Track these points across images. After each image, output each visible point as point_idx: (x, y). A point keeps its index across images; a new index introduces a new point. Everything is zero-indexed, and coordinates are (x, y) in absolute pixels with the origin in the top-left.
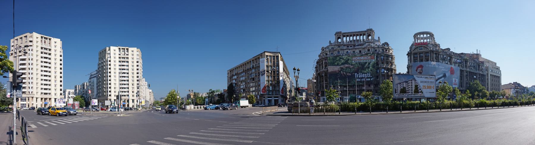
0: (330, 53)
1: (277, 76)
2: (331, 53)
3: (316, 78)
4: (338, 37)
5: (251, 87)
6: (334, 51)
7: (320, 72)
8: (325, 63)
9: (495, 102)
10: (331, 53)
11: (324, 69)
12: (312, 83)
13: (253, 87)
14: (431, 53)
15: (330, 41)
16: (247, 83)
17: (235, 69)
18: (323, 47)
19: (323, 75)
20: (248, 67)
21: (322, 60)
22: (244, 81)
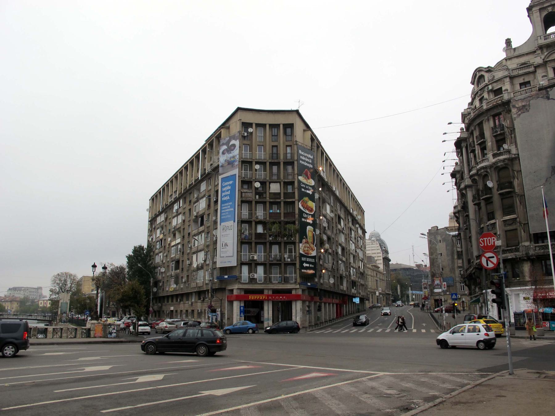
0: (512, 83)
1: (285, 202)
2: (521, 85)
3: (458, 212)
4: (545, 13)
5: (194, 253)
6: (534, 72)
7: (477, 174)
8: (494, 129)
9: (279, 326)
10: (521, 85)
11: (494, 156)
12: (444, 240)
13: (201, 251)
14: (501, 310)
15: (508, 42)
16: (186, 236)
17: (164, 189)
18: (479, 70)
19: (490, 184)
20: (190, 180)
21: (478, 121)
22: (179, 230)
